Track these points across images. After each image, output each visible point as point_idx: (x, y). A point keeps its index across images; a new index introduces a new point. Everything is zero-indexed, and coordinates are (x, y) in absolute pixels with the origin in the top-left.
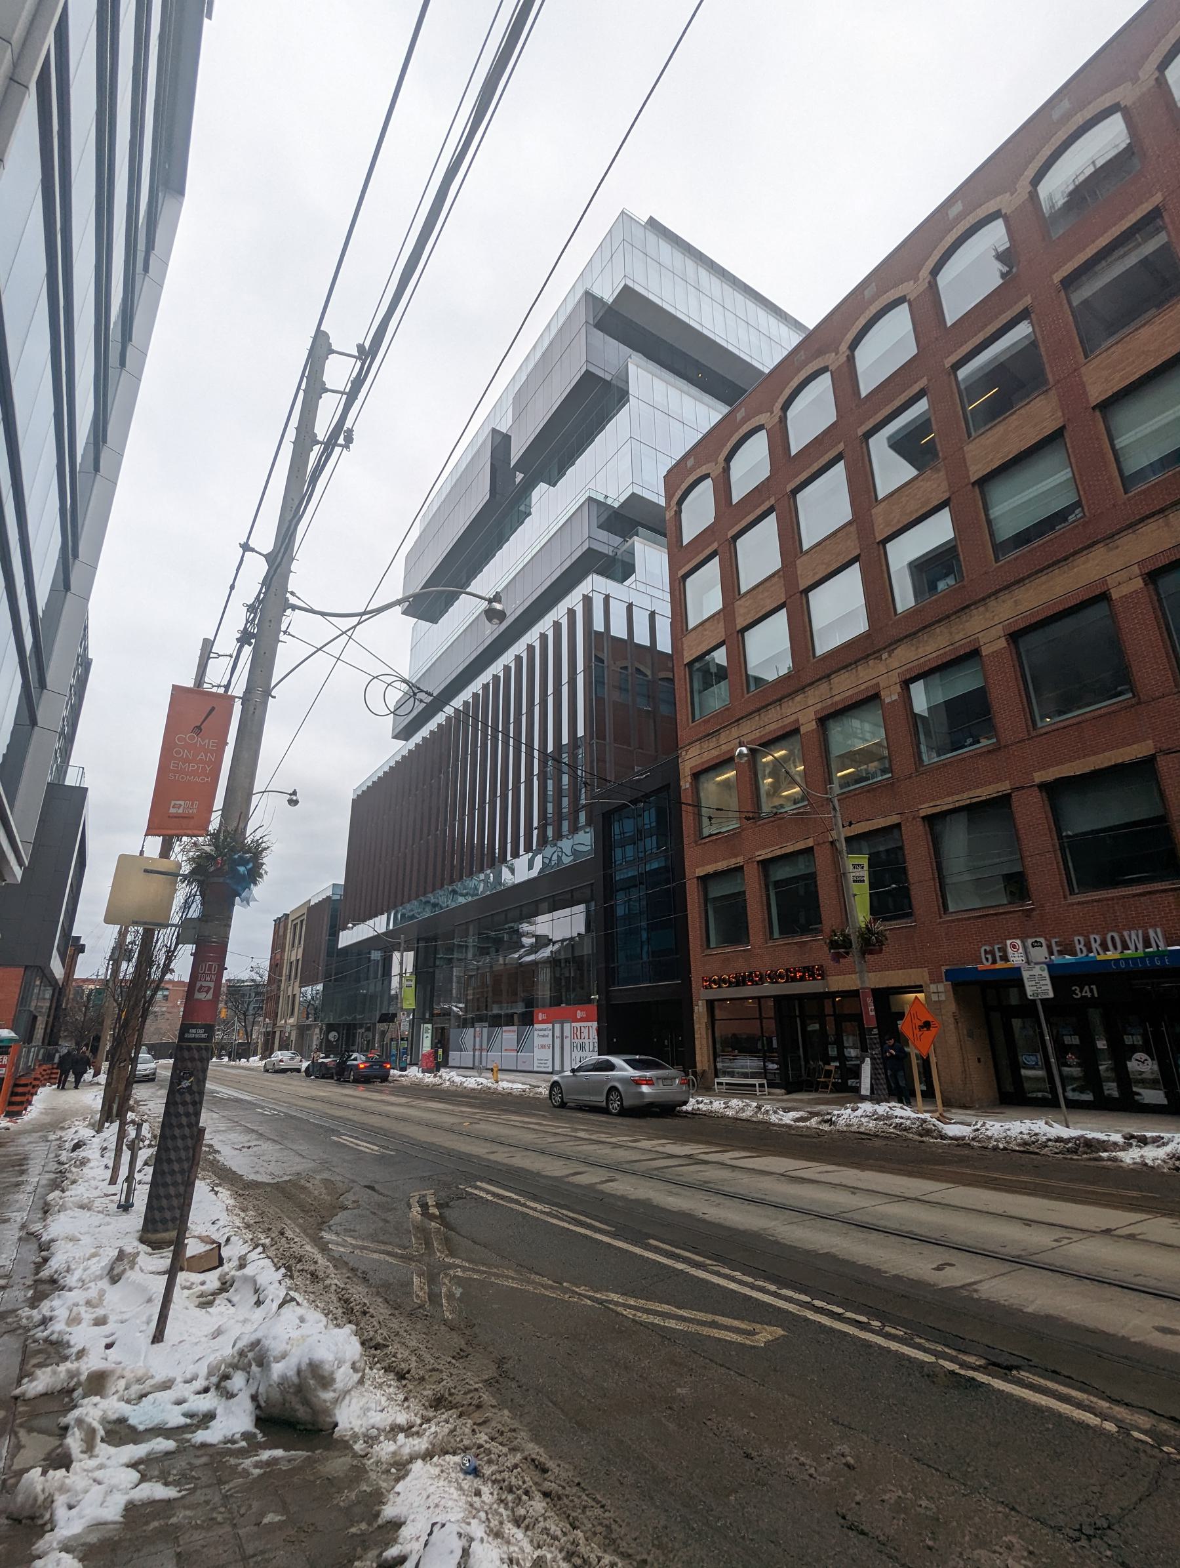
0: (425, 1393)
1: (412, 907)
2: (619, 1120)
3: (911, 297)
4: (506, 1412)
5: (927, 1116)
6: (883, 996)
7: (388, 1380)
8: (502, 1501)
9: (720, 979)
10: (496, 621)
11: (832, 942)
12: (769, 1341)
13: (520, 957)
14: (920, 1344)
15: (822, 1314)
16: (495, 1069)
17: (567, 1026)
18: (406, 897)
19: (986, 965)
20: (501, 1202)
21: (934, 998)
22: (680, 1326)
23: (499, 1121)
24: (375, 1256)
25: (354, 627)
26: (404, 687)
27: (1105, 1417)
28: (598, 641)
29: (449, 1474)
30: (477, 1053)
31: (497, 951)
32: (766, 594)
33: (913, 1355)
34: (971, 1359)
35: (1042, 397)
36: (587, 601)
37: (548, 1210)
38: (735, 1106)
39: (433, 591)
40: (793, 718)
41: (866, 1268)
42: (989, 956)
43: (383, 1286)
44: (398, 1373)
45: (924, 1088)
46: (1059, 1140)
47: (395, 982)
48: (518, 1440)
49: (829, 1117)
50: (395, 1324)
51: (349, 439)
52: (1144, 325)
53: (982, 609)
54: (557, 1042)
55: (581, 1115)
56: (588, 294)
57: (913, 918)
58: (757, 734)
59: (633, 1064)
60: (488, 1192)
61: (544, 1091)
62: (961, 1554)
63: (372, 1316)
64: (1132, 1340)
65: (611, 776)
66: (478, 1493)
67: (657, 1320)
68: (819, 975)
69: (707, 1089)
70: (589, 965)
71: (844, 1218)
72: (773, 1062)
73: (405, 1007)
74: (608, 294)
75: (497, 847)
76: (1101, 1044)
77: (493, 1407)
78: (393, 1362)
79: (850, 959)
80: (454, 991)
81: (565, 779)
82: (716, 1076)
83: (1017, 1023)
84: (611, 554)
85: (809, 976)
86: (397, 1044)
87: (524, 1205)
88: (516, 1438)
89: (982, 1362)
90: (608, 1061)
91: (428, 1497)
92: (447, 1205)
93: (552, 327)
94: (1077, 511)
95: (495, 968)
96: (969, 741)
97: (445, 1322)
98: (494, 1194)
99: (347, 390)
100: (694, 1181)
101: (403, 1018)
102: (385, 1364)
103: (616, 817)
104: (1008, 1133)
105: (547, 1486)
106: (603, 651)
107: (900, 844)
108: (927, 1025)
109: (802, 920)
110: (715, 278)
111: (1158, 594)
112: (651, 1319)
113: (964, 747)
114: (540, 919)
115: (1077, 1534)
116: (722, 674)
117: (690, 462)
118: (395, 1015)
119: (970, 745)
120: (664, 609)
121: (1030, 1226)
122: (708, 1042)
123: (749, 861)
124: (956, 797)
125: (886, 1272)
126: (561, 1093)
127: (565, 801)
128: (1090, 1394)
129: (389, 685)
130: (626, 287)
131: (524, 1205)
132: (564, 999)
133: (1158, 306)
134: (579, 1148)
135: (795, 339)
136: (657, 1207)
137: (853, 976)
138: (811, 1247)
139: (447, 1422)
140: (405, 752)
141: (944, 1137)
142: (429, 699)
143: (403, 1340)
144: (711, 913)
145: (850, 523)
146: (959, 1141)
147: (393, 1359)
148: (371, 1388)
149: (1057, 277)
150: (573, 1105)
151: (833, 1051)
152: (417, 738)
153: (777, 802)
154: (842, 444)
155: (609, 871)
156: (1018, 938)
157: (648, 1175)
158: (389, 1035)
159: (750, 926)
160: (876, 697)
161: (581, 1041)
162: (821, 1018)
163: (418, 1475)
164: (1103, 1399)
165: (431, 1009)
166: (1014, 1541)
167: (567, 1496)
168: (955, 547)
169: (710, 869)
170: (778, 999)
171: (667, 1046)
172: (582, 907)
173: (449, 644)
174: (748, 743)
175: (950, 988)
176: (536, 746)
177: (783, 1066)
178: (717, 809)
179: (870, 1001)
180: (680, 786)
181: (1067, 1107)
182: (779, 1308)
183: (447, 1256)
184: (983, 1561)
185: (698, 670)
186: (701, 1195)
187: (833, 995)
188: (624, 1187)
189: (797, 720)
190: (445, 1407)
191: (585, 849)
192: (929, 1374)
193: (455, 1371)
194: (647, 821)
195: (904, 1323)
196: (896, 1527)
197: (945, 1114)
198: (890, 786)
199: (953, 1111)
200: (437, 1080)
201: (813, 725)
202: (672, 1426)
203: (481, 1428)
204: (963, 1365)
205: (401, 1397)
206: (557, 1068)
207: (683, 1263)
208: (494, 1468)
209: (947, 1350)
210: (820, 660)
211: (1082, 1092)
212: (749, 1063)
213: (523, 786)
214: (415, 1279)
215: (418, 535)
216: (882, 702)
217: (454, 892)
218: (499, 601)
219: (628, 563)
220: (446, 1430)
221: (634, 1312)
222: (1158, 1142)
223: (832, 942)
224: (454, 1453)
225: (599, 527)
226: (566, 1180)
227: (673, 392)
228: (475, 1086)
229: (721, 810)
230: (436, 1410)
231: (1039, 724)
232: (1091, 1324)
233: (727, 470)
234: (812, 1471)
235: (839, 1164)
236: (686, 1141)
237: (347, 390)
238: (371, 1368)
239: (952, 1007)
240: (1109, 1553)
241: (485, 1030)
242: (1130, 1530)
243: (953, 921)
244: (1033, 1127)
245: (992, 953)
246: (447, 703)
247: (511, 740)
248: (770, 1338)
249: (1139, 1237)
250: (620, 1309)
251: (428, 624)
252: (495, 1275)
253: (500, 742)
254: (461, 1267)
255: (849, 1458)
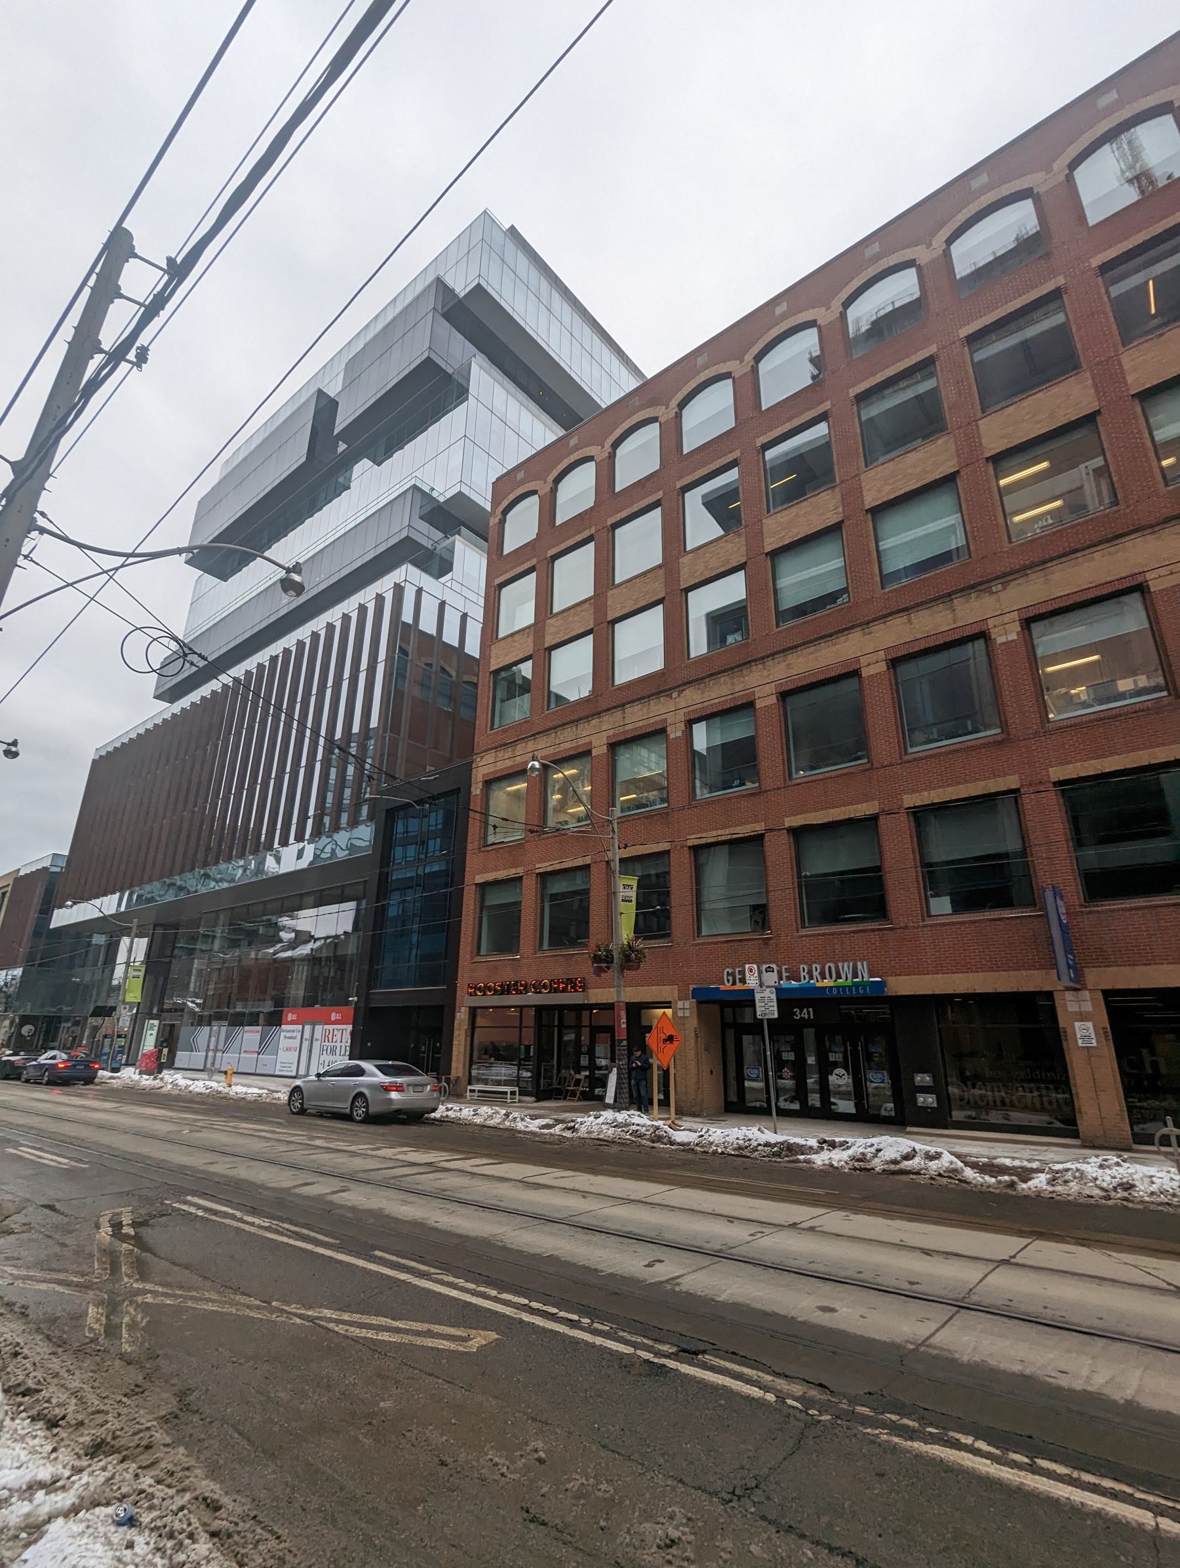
0: (81, 1440)
1: (154, 889)
2: (363, 1127)
3: (736, 375)
4: (181, 1450)
5: (660, 1123)
6: (635, 1010)
7: (34, 1430)
8: (158, 1549)
9: (485, 986)
10: (292, 593)
11: (595, 956)
12: (482, 1346)
13: (274, 954)
14: (622, 1337)
15: (537, 1315)
16: (229, 1072)
17: (319, 1028)
18: (146, 877)
19: (728, 986)
20: (214, 1218)
21: (680, 1014)
22: (394, 1338)
23: (226, 1128)
24: (43, 1287)
25: (117, 569)
26: (174, 646)
27: (766, 1388)
28: (404, 633)
29: (96, 1529)
30: (211, 1054)
31: (250, 944)
32: (576, 618)
33: (615, 1348)
34: (665, 1348)
35: (829, 492)
36: (398, 590)
37: (267, 1224)
38: (487, 1114)
39: (224, 548)
40: (587, 740)
41: (586, 1269)
42: (730, 978)
43: (45, 1321)
44: (49, 1420)
45: (662, 1097)
46: (767, 1144)
47: (119, 971)
48: (191, 1479)
49: (572, 1124)
50: (55, 1364)
51: (142, 357)
52: (912, 451)
53: (760, 666)
54: (306, 1044)
55: (320, 1122)
56: (439, 282)
57: (670, 939)
58: (551, 751)
59: (384, 1070)
60: (199, 1207)
61: (283, 1097)
62: (629, 1530)
63: (25, 1358)
64: (799, 1319)
65: (400, 773)
66: (130, 1545)
67: (370, 1334)
68: (580, 987)
69: (456, 1094)
70: (352, 964)
71: (571, 1221)
72: (527, 1070)
73: (128, 1000)
74: (461, 288)
75: (264, 832)
76: (811, 1060)
77: (166, 1445)
78: (45, 1408)
79: (609, 974)
80: (192, 985)
81: (351, 770)
82: (470, 1084)
83: (747, 1039)
84: (430, 547)
85: (572, 987)
86: (112, 1041)
87: (241, 1220)
88: (189, 1477)
89: (673, 1350)
90: (358, 1066)
91: (65, 1559)
92: (144, 1224)
93: (398, 303)
94: (844, 596)
95: (244, 963)
96: (737, 782)
97: (121, 1356)
98: (206, 1209)
99: (147, 303)
100: (433, 1190)
101: (123, 1012)
102: (34, 1412)
103: (402, 813)
104: (727, 1138)
105: (217, 1525)
106: (409, 644)
107: (667, 870)
108: (670, 1039)
109: (573, 934)
110: (567, 306)
111: (896, 680)
112: (364, 1333)
113: (732, 787)
114: (302, 913)
115: (730, 1496)
116: (525, 687)
117: (520, 475)
118: (114, 1009)
119: (737, 786)
120: (477, 613)
121: (732, 1222)
122: (465, 1050)
123: (527, 873)
124: (719, 832)
125: (602, 1271)
126: (302, 1099)
127: (348, 792)
128: (758, 1370)
129: (154, 640)
130: (479, 285)
131: (241, 1220)
132: (320, 999)
133: (925, 437)
134: (313, 1157)
135: (633, 384)
136: (388, 1216)
137: (612, 989)
138: (537, 1251)
139: (104, 1469)
140: (168, 716)
141: (672, 1143)
142: (202, 663)
143: (63, 1382)
144: (485, 919)
145: (659, 567)
146: (686, 1147)
147: (46, 1405)
148: (9, 1443)
149: (853, 392)
150: (313, 1111)
151: (584, 1061)
152: (185, 702)
153: (562, 818)
154: (661, 492)
155: (385, 870)
156: (756, 963)
157: (385, 1184)
158: (103, 1031)
159: (522, 937)
160: (662, 731)
161: (332, 1044)
162: (578, 1028)
163: (55, 1536)
164: (768, 1374)
165: (161, 1003)
166: (677, 1510)
167: (239, 1533)
168: (745, 607)
169: (490, 876)
170: (540, 1009)
171: (424, 1052)
172: (352, 905)
173: (239, 605)
174: (542, 758)
175: (695, 1005)
176: (323, 733)
177: (536, 1077)
178: (503, 819)
179: (623, 1014)
180: (470, 792)
181: (777, 1115)
182: (497, 1312)
183: (137, 1281)
184: (647, 1533)
185: (504, 678)
186: (436, 1203)
187: (591, 1007)
188: (357, 1197)
189: (590, 743)
190: (104, 1452)
191: (364, 844)
192: (625, 1364)
193: (124, 1411)
194: (432, 822)
195: (609, 1318)
196: (574, 1514)
197: (676, 1122)
198: (664, 815)
199: (684, 1118)
200: (157, 1083)
201: (604, 750)
202: (368, 1442)
203: (145, 1472)
204: (658, 1354)
205: (49, 1448)
206: (302, 1072)
207: (407, 1273)
208: (155, 1513)
209: (645, 1341)
210: (619, 689)
211: (791, 1102)
212: (504, 1071)
213: (287, 777)
214: (92, 1310)
215: (216, 481)
216: (667, 736)
217: (207, 876)
218: (299, 573)
219: (447, 560)
220: (101, 1479)
221: (346, 1327)
222: (844, 1145)
223: (595, 956)
224: (108, 1504)
225: (421, 518)
226: (293, 1191)
227: (512, 402)
228: (203, 1090)
229: (507, 820)
230: (92, 1458)
231: (794, 776)
232: (769, 1308)
233: (554, 491)
234: (504, 1470)
235: (575, 1170)
236: (428, 1149)
237: (147, 303)
238: (13, 1419)
239: (694, 1023)
240: (753, 1510)
241: (224, 1029)
242: (773, 1486)
243: (704, 944)
244: (748, 1133)
245: (733, 974)
246: (223, 671)
247: (295, 723)
248: (484, 1342)
249: (818, 1229)
250: (331, 1326)
251: (461, 409)
252: (192, 1298)
253: (282, 724)
254: (152, 1293)
255: (541, 1453)
